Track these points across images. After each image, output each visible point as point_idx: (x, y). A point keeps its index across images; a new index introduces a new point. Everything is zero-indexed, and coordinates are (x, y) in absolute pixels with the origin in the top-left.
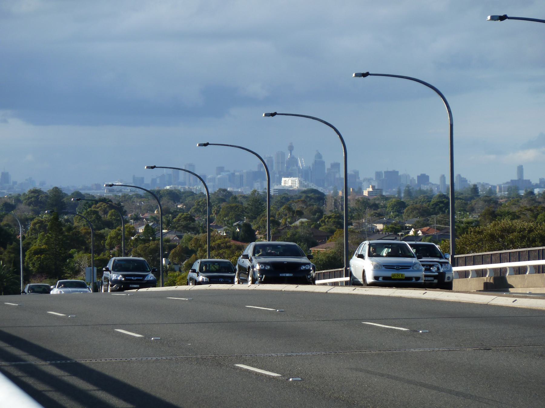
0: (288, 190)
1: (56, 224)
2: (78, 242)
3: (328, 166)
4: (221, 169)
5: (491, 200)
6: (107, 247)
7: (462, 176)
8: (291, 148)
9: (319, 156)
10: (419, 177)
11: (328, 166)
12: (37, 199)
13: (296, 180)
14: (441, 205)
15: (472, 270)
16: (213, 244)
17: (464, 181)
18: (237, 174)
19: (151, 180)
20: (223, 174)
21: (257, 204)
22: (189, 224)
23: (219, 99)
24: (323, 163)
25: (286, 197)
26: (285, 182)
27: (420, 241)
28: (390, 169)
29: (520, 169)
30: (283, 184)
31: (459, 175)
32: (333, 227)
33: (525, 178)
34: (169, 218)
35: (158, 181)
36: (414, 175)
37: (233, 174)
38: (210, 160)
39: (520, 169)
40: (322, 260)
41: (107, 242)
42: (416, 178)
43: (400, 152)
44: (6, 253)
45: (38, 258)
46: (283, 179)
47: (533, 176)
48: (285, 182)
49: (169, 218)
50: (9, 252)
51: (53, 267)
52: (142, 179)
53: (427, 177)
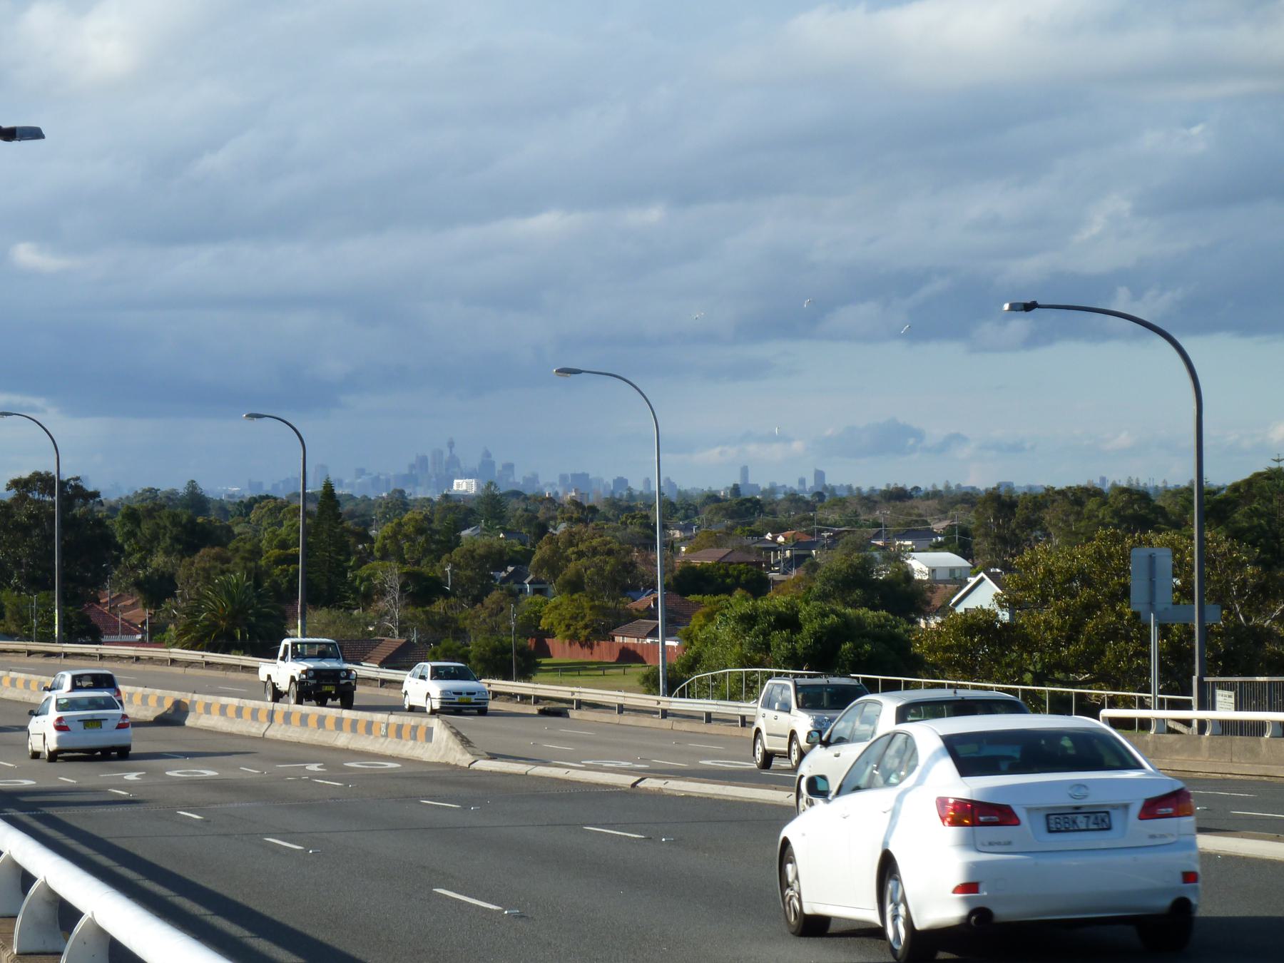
0: (464, 496)
3: (498, 467)
4: (361, 472)
6: (377, 554)
7: (673, 480)
8: (451, 445)
10: (615, 481)
11: (498, 467)
13: (473, 482)
14: (748, 505)
16: (582, 547)
20: (364, 479)
24: (492, 464)
26: (458, 485)
28: (580, 472)
29: (745, 471)
30: (455, 488)
31: (668, 479)
32: (849, 510)
33: (752, 481)
35: (281, 487)
36: (609, 479)
37: (378, 478)
39: (745, 471)
40: (839, 571)
41: (376, 545)
44: (237, 560)
45: (283, 570)
48: (458, 485)
50: (243, 558)
52: (260, 484)
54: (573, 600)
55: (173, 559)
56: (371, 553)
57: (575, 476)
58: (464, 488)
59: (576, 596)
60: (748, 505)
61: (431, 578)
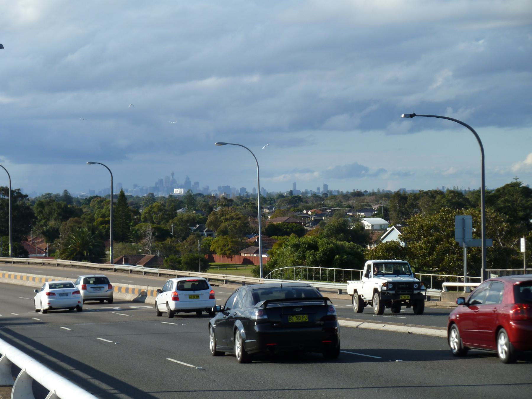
3: (192, 183)
4: (135, 186)
8: (173, 174)
9: (188, 178)
13: (182, 190)
15: (109, 263)
17: (265, 191)
18: (144, 188)
24: (190, 182)
27: (480, 196)
29: (295, 185)
30: (175, 192)
31: (263, 188)
33: (297, 189)
35: (103, 192)
37: (142, 188)
39: (295, 185)
40: (334, 226)
42: (239, 190)
44: (85, 222)
45: (103, 227)
46: (175, 190)
51: (121, 233)
53: (245, 189)
54: (224, 239)
58: (178, 192)
59: (225, 237)
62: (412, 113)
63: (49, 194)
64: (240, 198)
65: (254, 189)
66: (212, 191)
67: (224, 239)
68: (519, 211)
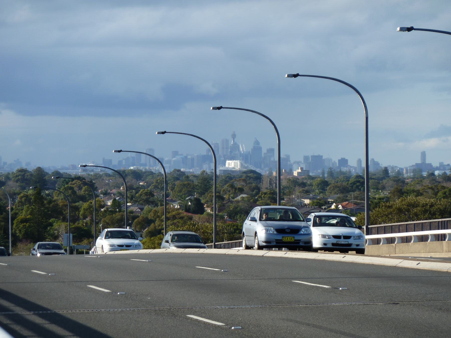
1: (39, 198)
2: (57, 212)
3: (264, 151)
4: (175, 153)
5: (399, 180)
7: (375, 160)
8: (234, 136)
9: (257, 143)
11: (264, 151)
12: (23, 177)
13: (238, 162)
16: (168, 215)
17: (377, 164)
18: (189, 157)
19: (118, 162)
20: (178, 157)
21: (206, 182)
22: (149, 199)
23: (176, 95)
24: (260, 149)
25: (230, 177)
29: (423, 155)
30: (227, 166)
31: (373, 159)
33: (428, 162)
34: (132, 194)
36: (336, 159)
37: (186, 157)
38: (167, 145)
39: (423, 155)
41: (81, 213)
42: (337, 162)
43: (324, 140)
47: (434, 161)
48: (229, 164)
49: (132, 194)
54: (151, 240)
55: (328, 188)
56: (79, 216)
57: (313, 157)
58: (233, 166)
59: (152, 238)
60: (358, 184)
61: (85, 230)
62: (163, 131)
63: (431, 164)
64: (419, 179)
65: (359, 161)
66: (295, 162)
67: (151, 240)
68: (360, 185)
